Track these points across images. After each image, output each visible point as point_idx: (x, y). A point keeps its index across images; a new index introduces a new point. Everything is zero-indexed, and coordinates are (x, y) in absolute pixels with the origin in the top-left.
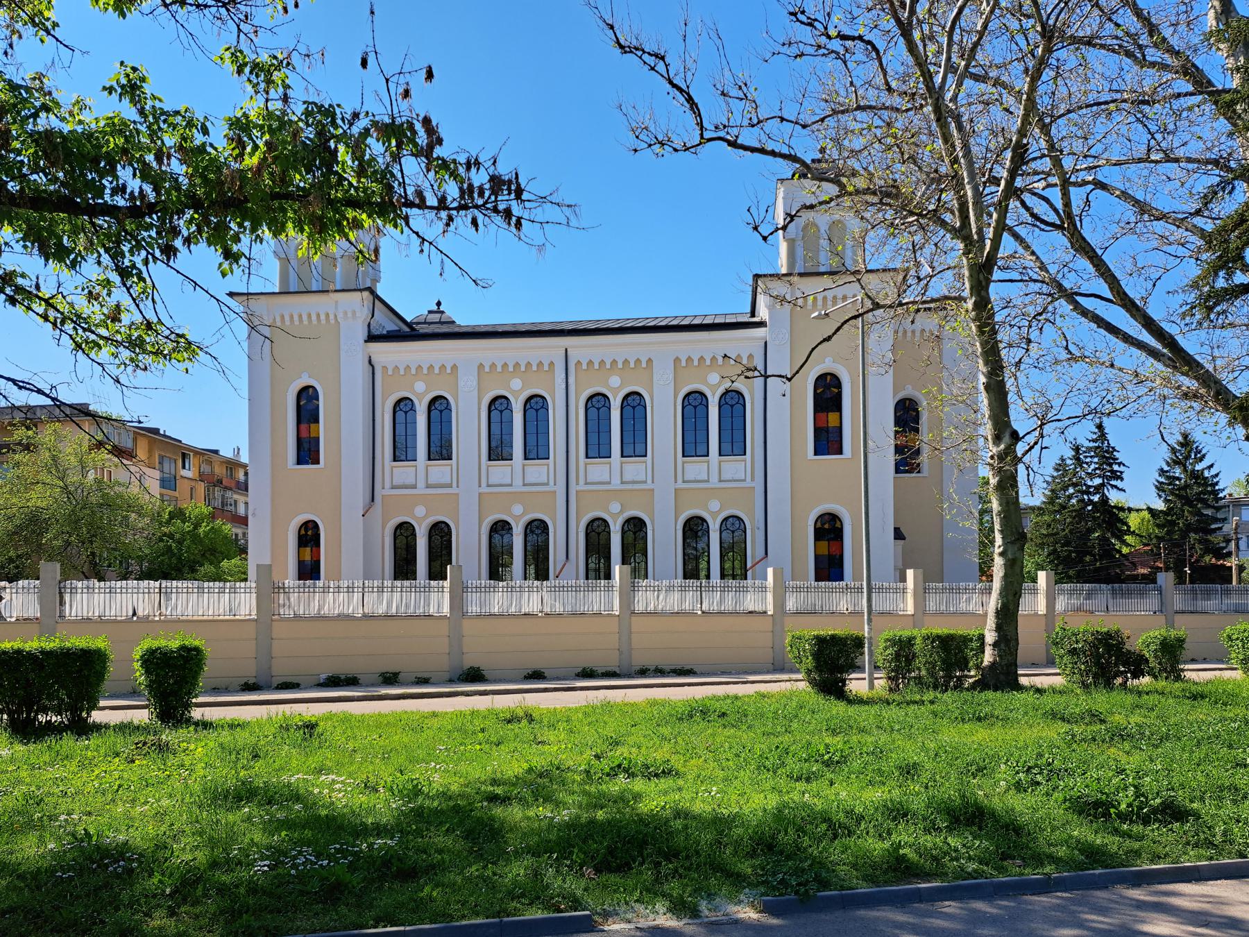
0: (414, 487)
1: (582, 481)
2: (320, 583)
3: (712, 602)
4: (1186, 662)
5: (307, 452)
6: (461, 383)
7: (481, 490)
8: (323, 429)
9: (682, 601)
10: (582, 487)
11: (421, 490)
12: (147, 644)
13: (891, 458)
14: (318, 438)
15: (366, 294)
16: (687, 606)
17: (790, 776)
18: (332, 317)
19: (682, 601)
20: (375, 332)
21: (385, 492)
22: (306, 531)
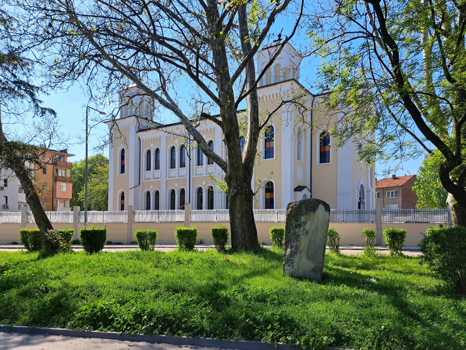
0: (150, 179)
1: (194, 174)
2: (57, 212)
3: (163, 218)
4: (196, 245)
5: (123, 171)
6: (162, 143)
7: (167, 179)
8: (275, 144)
9: (152, 218)
10: (194, 176)
11: (152, 180)
12: (274, 228)
13: (109, 173)
14: (273, 147)
15: (134, 117)
16: (154, 220)
17: (147, 273)
18: (278, 95)
19: (152, 218)
20: (141, 128)
21: (143, 181)
22: (268, 186)
